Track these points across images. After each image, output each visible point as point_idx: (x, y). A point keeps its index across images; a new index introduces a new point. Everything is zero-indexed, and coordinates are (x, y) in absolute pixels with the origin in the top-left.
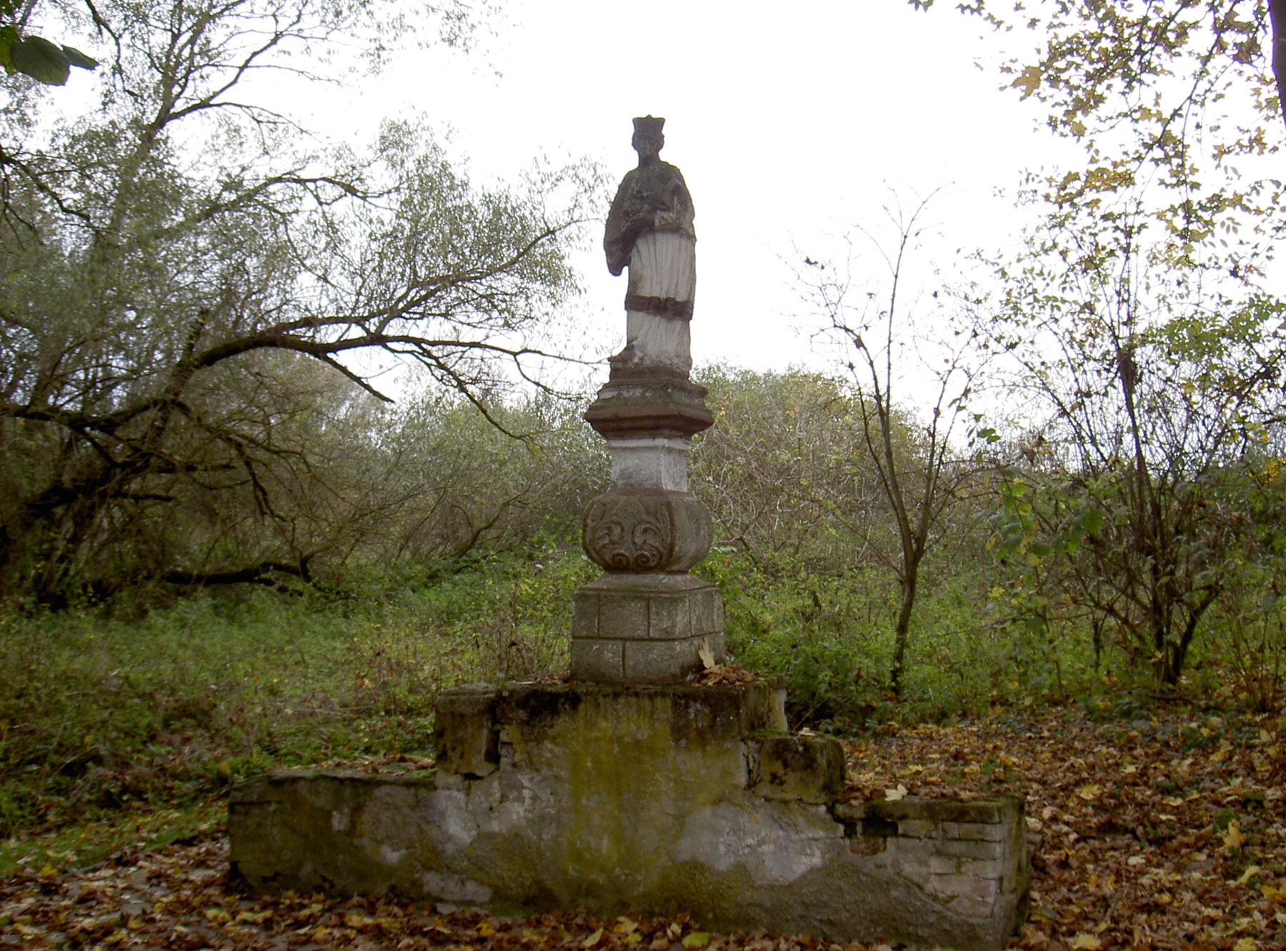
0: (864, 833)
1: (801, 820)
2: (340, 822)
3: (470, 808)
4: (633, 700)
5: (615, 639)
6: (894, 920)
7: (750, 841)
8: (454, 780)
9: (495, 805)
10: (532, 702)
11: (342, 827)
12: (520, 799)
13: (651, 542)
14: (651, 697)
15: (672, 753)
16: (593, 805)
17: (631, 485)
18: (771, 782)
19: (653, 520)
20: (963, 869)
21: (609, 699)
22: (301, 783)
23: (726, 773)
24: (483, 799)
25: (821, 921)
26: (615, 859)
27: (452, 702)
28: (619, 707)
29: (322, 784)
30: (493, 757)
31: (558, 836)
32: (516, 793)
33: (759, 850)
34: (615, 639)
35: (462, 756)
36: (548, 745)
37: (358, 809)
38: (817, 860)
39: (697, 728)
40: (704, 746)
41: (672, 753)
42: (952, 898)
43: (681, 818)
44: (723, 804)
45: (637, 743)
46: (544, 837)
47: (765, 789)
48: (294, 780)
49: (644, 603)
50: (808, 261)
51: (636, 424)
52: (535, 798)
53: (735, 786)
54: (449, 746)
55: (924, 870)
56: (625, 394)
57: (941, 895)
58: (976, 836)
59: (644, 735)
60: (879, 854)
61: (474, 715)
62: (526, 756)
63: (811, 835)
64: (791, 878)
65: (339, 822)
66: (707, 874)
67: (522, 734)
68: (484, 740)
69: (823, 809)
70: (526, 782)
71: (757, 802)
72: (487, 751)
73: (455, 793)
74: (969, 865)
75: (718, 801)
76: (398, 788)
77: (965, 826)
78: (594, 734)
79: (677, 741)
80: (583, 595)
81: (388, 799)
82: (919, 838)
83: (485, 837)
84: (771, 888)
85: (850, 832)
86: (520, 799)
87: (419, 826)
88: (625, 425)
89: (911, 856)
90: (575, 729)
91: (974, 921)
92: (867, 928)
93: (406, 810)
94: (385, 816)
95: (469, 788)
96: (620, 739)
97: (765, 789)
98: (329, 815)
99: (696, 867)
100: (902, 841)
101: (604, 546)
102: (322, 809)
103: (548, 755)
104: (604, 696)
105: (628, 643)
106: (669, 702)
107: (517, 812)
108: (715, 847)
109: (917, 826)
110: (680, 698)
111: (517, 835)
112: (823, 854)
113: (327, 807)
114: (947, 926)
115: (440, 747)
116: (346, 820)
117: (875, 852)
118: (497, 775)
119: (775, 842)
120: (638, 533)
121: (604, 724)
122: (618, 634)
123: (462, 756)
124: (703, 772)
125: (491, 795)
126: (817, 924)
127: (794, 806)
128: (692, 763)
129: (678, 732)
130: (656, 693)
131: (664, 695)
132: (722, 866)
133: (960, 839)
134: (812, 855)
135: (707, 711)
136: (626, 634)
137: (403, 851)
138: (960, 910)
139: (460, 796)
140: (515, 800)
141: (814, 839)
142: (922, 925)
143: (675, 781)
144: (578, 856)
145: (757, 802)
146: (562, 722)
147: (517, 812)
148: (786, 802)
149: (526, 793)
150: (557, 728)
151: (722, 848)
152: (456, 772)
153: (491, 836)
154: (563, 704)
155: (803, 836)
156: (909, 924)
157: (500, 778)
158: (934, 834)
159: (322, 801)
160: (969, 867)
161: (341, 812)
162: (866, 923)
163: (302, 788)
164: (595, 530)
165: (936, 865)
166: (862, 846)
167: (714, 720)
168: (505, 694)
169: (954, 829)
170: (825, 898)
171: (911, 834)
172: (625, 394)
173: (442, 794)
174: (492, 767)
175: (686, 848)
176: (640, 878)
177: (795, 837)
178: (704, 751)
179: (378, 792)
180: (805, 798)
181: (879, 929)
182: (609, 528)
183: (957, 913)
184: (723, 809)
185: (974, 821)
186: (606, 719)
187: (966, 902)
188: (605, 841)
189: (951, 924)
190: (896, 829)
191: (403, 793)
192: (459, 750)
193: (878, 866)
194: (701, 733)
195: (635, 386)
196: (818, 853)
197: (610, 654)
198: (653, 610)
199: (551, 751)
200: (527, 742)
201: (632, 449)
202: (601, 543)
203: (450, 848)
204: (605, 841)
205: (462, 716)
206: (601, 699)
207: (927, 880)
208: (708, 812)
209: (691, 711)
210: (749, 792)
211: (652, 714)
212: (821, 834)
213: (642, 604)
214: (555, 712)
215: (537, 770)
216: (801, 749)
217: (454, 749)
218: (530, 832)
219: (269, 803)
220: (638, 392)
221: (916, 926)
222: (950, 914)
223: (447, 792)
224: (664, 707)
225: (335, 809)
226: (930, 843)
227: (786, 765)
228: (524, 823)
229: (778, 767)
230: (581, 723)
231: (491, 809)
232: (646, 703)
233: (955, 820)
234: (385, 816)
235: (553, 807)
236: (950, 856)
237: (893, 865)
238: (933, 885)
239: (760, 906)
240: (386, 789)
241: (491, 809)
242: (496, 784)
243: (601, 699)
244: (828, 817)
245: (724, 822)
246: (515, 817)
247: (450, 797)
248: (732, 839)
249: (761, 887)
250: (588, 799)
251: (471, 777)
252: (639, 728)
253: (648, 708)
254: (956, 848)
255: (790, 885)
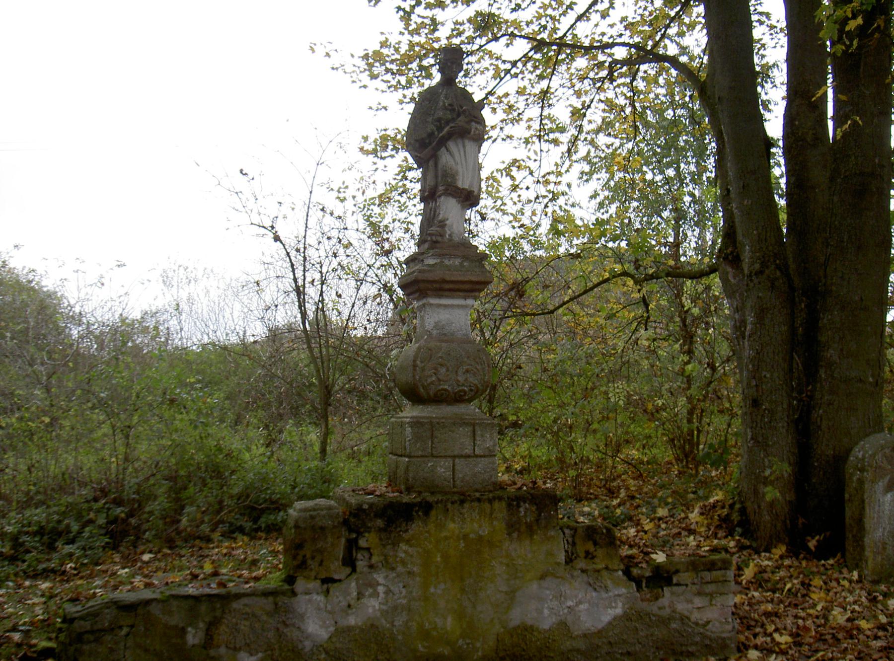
0: (647, 587)
1: (609, 582)
2: (194, 636)
3: (329, 607)
4: (476, 504)
5: (445, 457)
6: (672, 644)
7: (570, 603)
8: (315, 585)
9: (352, 603)
10: (390, 512)
11: (196, 641)
12: (376, 595)
13: (471, 380)
14: (490, 501)
15: (507, 543)
16: (439, 592)
17: (445, 335)
18: (586, 557)
19: (473, 363)
20: (714, 602)
21: (456, 505)
22: (154, 604)
23: (550, 554)
24: (341, 598)
25: (622, 654)
26: (458, 633)
27: (312, 517)
28: (465, 511)
29: (175, 603)
30: (350, 562)
31: (407, 622)
32: (371, 590)
33: (577, 608)
34: (445, 457)
35: (321, 564)
36: (403, 546)
37: (213, 625)
38: (619, 611)
39: (526, 523)
40: (531, 536)
41: (507, 543)
42: (708, 622)
43: (511, 594)
44: (548, 579)
45: (480, 538)
46: (396, 623)
47: (581, 564)
48: (148, 602)
49: (471, 428)
50: (241, 171)
51: (457, 287)
52: (388, 592)
53: (558, 564)
54: (308, 556)
55: (690, 606)
56: (447, 262)
57: (700, 622)
58: (721, 579)
59: (485, 531)
60: (660, 600)
61: (335, 527)
62: (382, 558)
63: (616, 593)
64: (600, 626)
65: (193, 637)
66: (535, 633)
67: (381, 539)
68: (342, 548)
69: (620, 573)
70: (381, 580)
71: (575, 574)
72: (343, 558)
73: (315, 597)
74: (718, 599)
75: (542, 577)
76: (258, 599)
77: (714, 572)
78: (443, 534)
79: (509, 534)
80: (418, 422)
81: (247, 609)
82: (687, 585)
83: (342, 632)
84: (585, 635)
85: (639, 587)
86: (376, 595)
87: (278, 629)
88: (447, 286)
89: (682, 597)
90: (428, 532)
91: (724, 635)
92: (654, 653)
93: (265, 618)
94: (244, 626)
95: (328, 591)
96: (465, 537)
97: (581, 564)
98: (183, 631)
99: (526, 629)
100: (675, 588)
101: (432, 383)
102: (177, 626)
103: (403, 555)
104: (453, 503)
105: (457, 460)
106: (504, 504)
107: (373, 606)
108: (540, 611)
109: (685, 577)
110: (513, 500)
111: (372, 625)
112: (624, 605)
113: (181, 625)
114: (708, 642)
115: (300, 558)
116: (201, 634)
117: (657, 599)
118: (355, 576)
119: (589, 602)
120: (460, 372)
121: (452, 526)
122: (449, 453)
123: (321, 564)
124: (530, 556)
125: (349, 594)
126: (618, 656)
127: (605, 573)
128: (522, 550)
129: (512, 527)
130: (494, 498)
131: (500, 499)
132: (546, 625)
133: (711, 582)
134: (616, 607)
135: (534, 508)
136: (456, 453)
137: (260, 655)
138: (714, 630)
139: (320, 598)
140: (370, 596)
141: (619, 595)
142: (691, 644)
143: (507, 565)
144: (425, 635)
145: (575, 574)
146: (416, 527)
147: (373, 606)
148: (598, 571)
149: (381, 589)
150: (411, 532)
151: (546, 612)
152: (316, 578)
153: (349, 629)
154: (417, 512)
155: (610, 594)
156: (681, 645)
157: (357, 579)
158: (696, 581)
159: (175, 620)
160: (719, 600)
161: (196, 628)
162: (653, 650)
163: (155, 609)
164: (423, 369)
165: (698, 602)
166: (648, 596)
167: (540, 515)
168: (366, 507)
169: (707, 576)
170: (625, 637)
171: (682, 582)
172: (447, 262)
173: (302, 598)
174: (348, 570)
175: (516, 617)
176: (478, 645)
177: (604, 595)
178: (532, 539)
179: (235, 605)
180: (610, 566)
181: (661, 652)
182: (436, 369)
183: (712, 632)
184: (549, 582)
185: (720, 569)
186: (454, 522)
187: (717, 624)
188: (449, 620)
189: (711, 640)
190: (671, 580)
191: (262, 601)
192: (318, 558)
193: (660, 608)
194: (529, 527)
195: (456, 256)
196: (620, 605)
197: (442, 470)
198: (479, 433)
199: (406, 552)
200: (384, 546)
201: (446, 306)
202: (429, 380)
203: (308, 644)
204: (449, 620)
205: (322, 528)
206: (449, 505)
207: (691, 613)
208: (535, 586)
209: (522, 509)
210: (568, 567)
211: (491, 514)
212: (624, 590)
213: (468, 429)
214: (409, 519)
215: (393, 569)
216: (604, 531)
217: (313, 558)
218: (384, 622)
219: (121, 627)
220: (457, 262)
221: (687, 645)
222: (709, 633)
223: (307, 597)
224: (500, 507)
225: (190, 625)
226: (694, 588)
227: (595, 544)
228: (378, 614)
229: (590, 547)
230: (431, 526)
231: (349, 606)
232: (487, 506)
233: (709, 570)
234: (244, 626)
235: (405, 597)
236: (706, 594)
237: (670, 606)
238: (695, 616)
239: (578, 651)
240: (245, 600)
241: (349, 606)
242: (353, 584)
243: (449, 505)
244: (625, 578)
245: (548, 592)
246: (370, 610)
247: (310, 601)
248: (555, 603)
249: (577, 636)
250: (435, 587)
251: (328, 581)
252: (480, 527)
253: (488, 510)
254: (710, 588)
255: (600, 632)
